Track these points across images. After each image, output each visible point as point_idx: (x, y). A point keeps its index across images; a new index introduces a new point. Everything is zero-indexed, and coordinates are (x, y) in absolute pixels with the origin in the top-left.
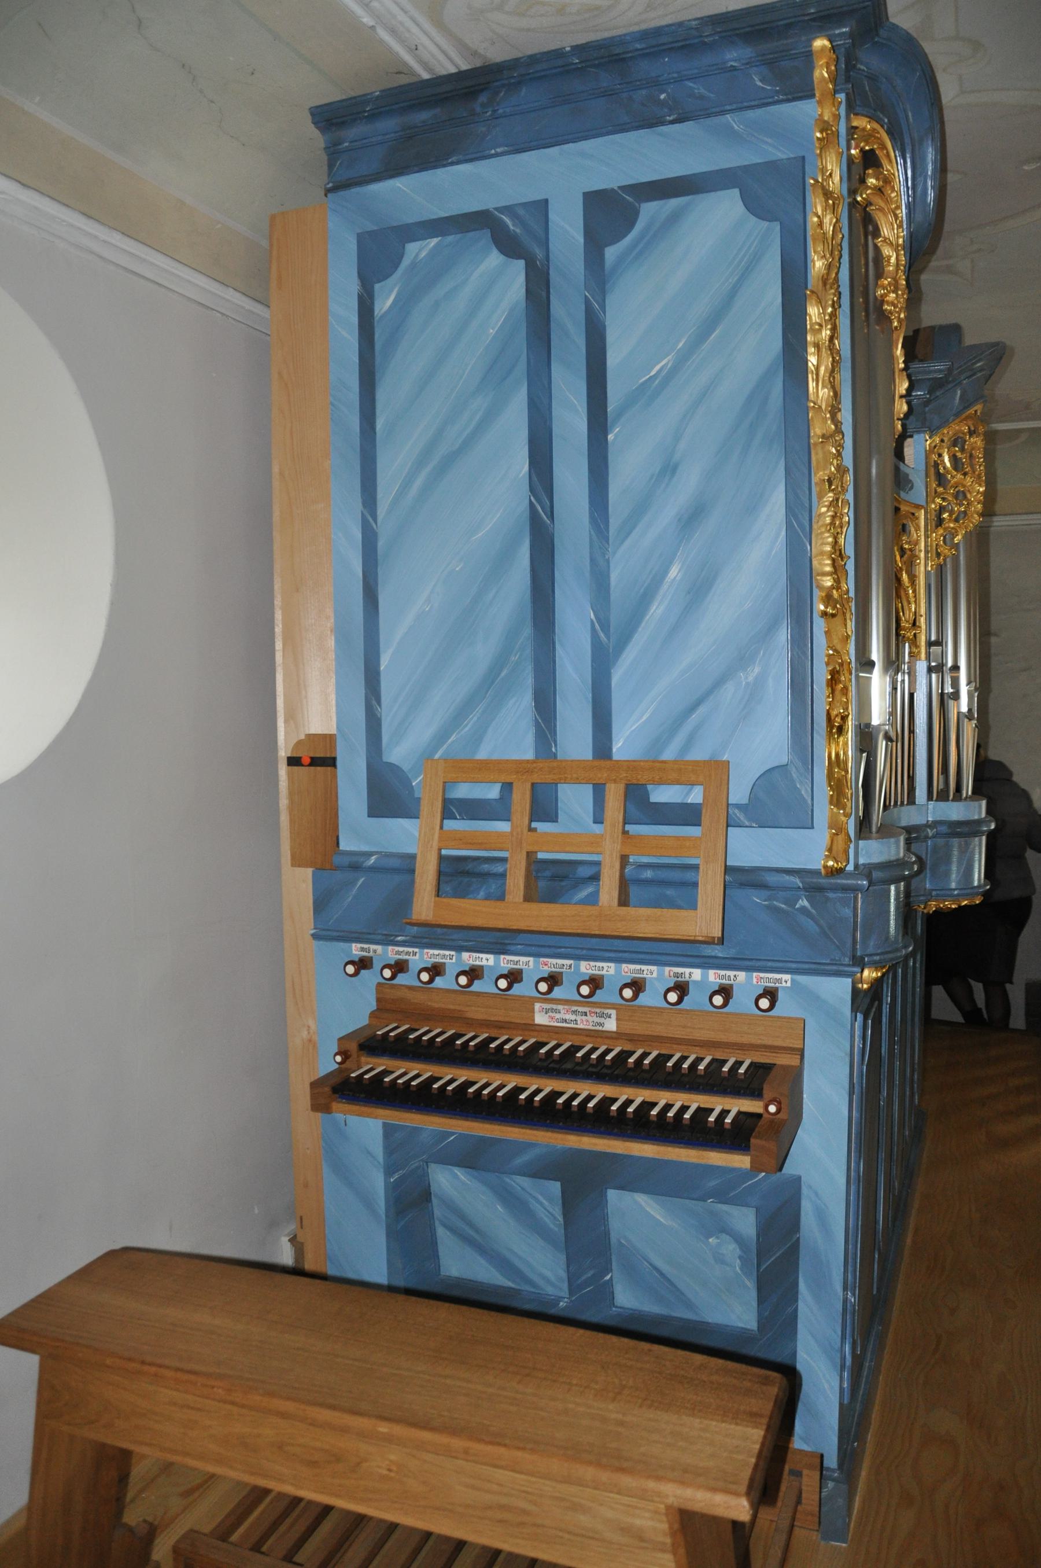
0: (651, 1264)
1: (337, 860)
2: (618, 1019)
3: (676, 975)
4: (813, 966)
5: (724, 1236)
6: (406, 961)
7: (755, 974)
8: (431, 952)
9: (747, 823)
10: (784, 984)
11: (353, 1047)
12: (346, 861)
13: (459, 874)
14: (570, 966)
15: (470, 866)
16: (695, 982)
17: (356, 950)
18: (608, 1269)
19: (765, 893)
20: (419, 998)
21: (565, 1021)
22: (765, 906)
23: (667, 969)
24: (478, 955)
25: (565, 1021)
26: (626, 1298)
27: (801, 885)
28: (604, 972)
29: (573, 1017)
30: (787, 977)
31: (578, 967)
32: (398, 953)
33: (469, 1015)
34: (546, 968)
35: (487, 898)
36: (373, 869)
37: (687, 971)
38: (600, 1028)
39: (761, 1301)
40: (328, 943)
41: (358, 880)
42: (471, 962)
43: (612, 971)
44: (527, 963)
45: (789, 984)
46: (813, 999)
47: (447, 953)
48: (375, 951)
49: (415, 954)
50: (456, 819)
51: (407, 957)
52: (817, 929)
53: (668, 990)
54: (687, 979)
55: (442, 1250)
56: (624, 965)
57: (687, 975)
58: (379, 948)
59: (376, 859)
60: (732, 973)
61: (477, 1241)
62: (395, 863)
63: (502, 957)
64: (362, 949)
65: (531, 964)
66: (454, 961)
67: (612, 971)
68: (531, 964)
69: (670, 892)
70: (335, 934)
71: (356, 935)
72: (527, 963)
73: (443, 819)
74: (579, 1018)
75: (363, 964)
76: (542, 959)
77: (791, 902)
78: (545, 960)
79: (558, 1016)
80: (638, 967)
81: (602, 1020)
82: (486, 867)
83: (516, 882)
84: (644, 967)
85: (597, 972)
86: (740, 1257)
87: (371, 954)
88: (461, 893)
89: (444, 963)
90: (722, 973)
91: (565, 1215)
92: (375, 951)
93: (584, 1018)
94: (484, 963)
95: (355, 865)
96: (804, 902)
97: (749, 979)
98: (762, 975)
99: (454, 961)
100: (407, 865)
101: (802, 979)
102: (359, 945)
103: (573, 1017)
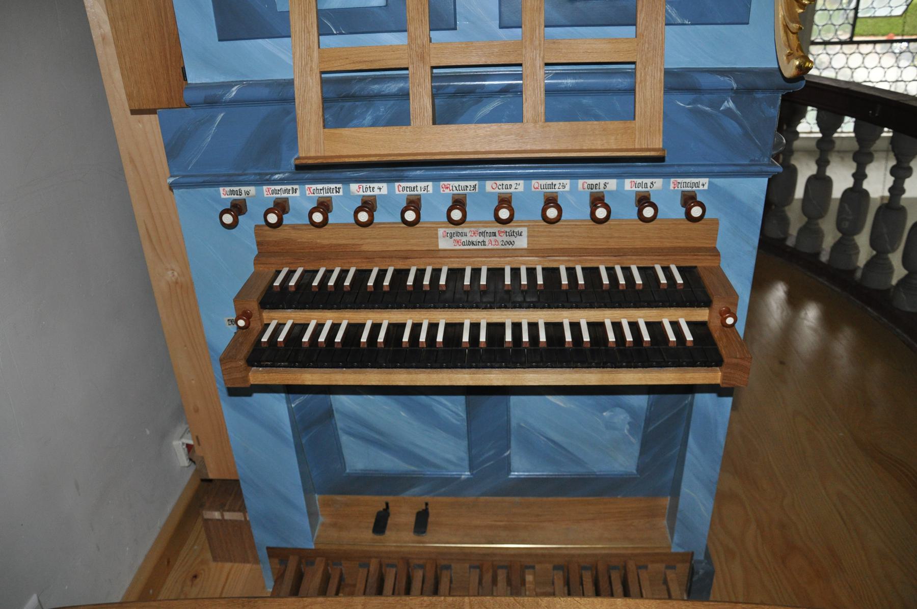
0: (547, 438)
1: (188, 96)
2: (528, 236)
3: (591, 187)
4: (738, 168)
5: (618, 410)
6: (286, 200)
7: (672, 180)
8: (314, 187)
9: (679, 21)
10: (701, 188)
11: (253, 306)
12: (200, 96)
13: (345, 97)
14: (475, 187)
15: (356, 88)
16: (610, 192)
17: (225, 193)
18: (508, 447)
19: (690, 97)
20: (313, 235)
21: (473, 243)
22: (689, 110)
23: (581, 182)
24: (368, 185)
25: (473, 243)
26: (521, 468)
27: (735, 86)
28: (512, 190)
29: (481, 239)
30: (705, 181)
31: (483, 187)
32: (274, 192)
33: (365, 248)
34: (447, 191)
35: (374, 124)
36: (234, 102)
37: (602, 182)
38: (510, 247)
39: (642, 452)
40: (191, 191)
41: (216, 117)
42: (361, 193)
43: (521, 188)
44: (426, 188)
45: (706, 187)
46: (729, 200)
47: (333, 186)
48: (247, 193)
49: (295, 191)
50: (333, 34)
51: (286, 195)
52: (740, 130)
53: (450, 211)
54: (602, 189)
55: (346, 452)
56: (534, 182)
57: (602, 186)
58: (252, 190)
59: (238, 90)
60: (648, 181)
61: (376, 439)
62: (264, 93)
63: (397, 184)
64: (232, 192)
65: (430, 189)
66: (341, 193)
67: (521, 188)
68: (430, 189)
69: (586, 101)
70: (200, 180)
71: (224, 178)
72: (426, 188)
73: (319, 35)
74: (487, 239)
75: (238, 208)
76: (442, 183)
77: (716, 105)
78: (446, 183)
79: (464, 239)
80: (549, 182)
81: (512, 239)
82: (376, 87)
83: (421, 102)
84: (555, 182)
85: (505, 191)
86: (629, 423)
87: (243, 196)
88: (401, 89)
89: (331, 197)
90: (639, 181)
91: (468, 413)
92: (247, 193)
93: (493, 238)
94: (376, 192)
95: (212, 99)
96: (730, 104)
97: (666, 186)
98: (679, 180)
99: (341, 193)
100: (282, 95)
101: (720, 182)
102: (228, 189)
103: (481, 239)
